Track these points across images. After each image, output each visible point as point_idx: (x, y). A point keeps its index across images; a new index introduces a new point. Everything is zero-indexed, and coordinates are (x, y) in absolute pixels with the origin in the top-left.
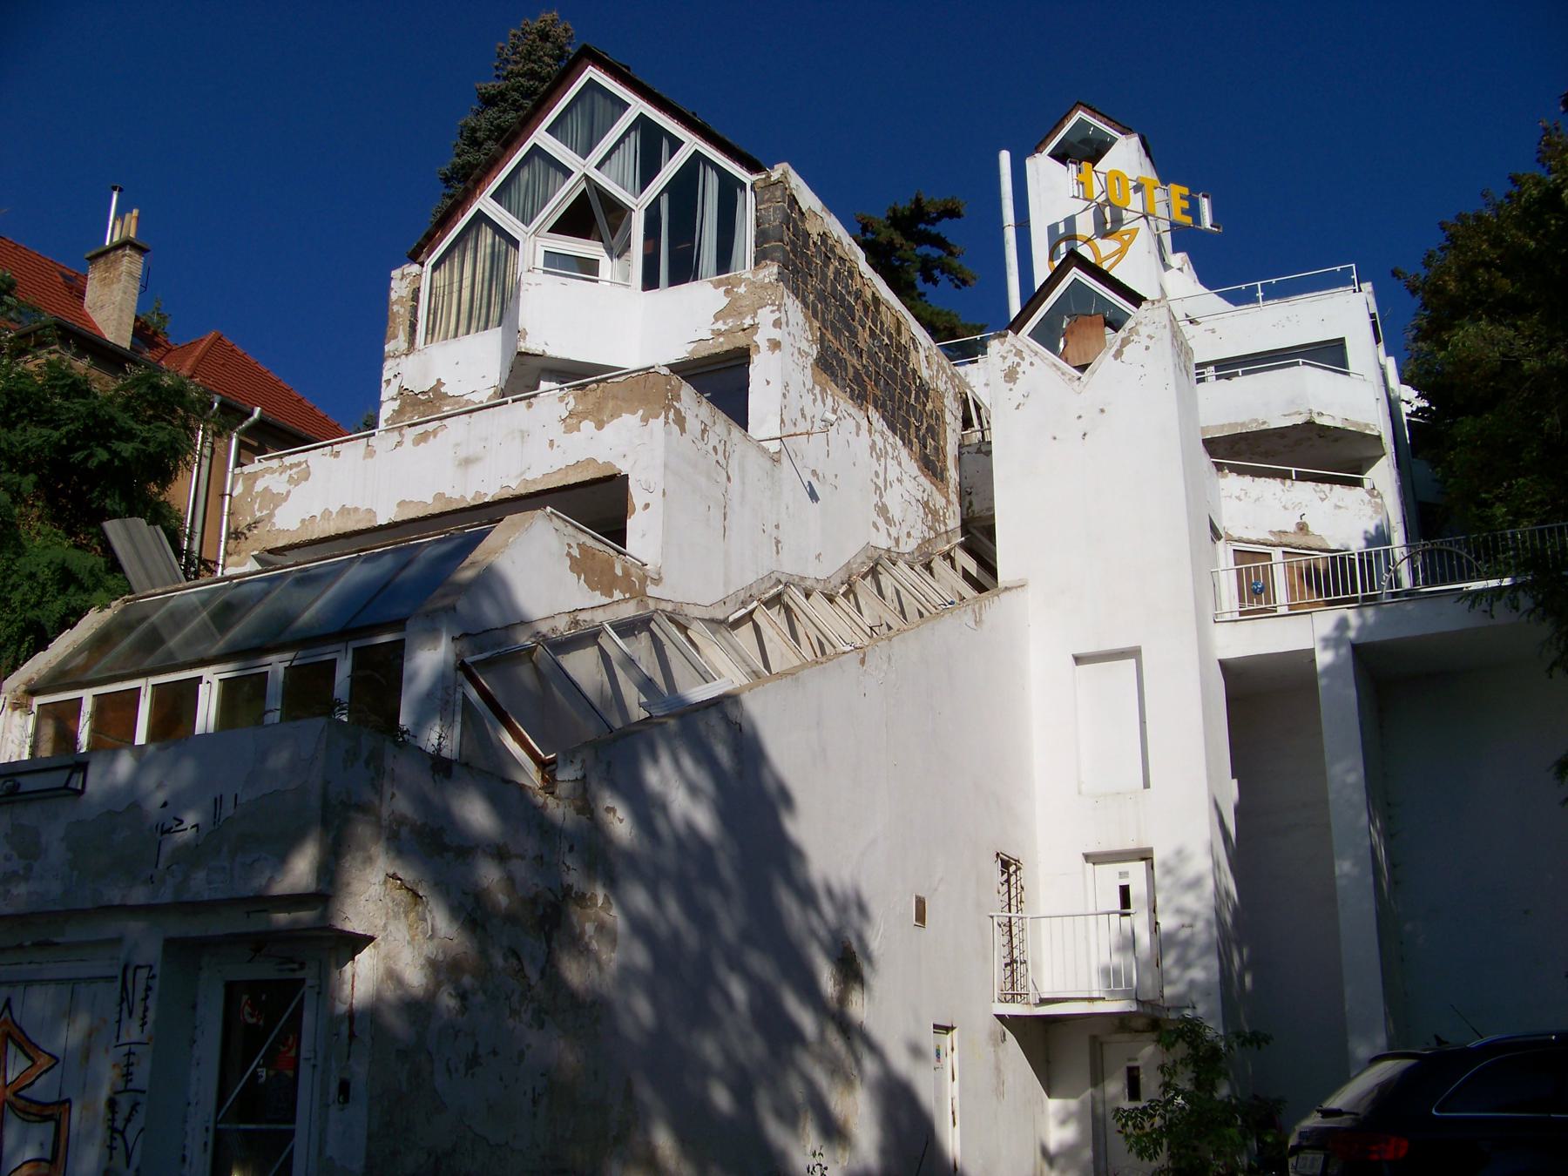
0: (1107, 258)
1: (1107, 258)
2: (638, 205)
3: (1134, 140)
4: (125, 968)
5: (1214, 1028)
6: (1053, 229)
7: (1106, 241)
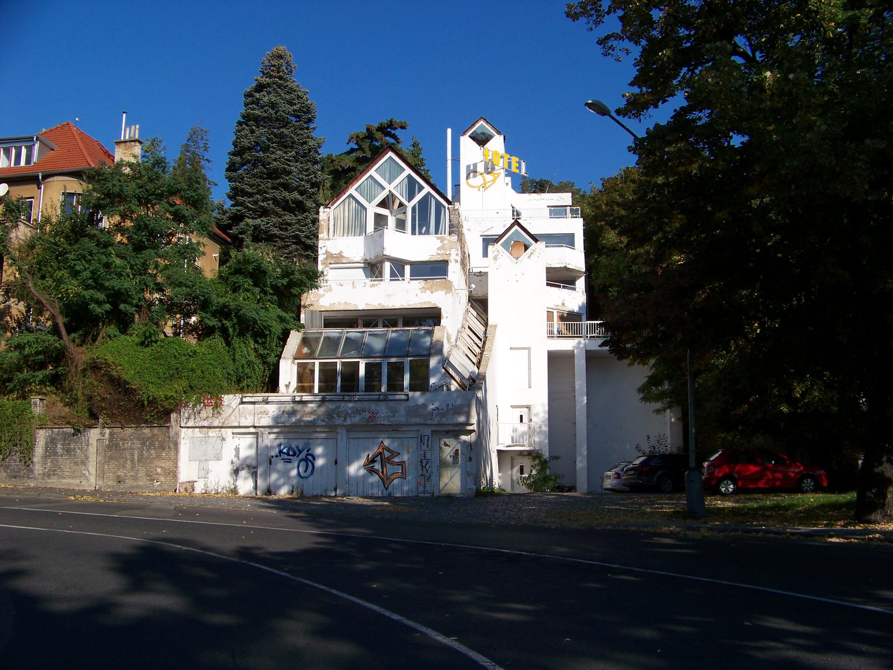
0: (488, 182)
1: (488, 182)
2: (410, 206)
3: (502, 137)
4: (421, 436)
5: (546, 455)
6: (468, 167)
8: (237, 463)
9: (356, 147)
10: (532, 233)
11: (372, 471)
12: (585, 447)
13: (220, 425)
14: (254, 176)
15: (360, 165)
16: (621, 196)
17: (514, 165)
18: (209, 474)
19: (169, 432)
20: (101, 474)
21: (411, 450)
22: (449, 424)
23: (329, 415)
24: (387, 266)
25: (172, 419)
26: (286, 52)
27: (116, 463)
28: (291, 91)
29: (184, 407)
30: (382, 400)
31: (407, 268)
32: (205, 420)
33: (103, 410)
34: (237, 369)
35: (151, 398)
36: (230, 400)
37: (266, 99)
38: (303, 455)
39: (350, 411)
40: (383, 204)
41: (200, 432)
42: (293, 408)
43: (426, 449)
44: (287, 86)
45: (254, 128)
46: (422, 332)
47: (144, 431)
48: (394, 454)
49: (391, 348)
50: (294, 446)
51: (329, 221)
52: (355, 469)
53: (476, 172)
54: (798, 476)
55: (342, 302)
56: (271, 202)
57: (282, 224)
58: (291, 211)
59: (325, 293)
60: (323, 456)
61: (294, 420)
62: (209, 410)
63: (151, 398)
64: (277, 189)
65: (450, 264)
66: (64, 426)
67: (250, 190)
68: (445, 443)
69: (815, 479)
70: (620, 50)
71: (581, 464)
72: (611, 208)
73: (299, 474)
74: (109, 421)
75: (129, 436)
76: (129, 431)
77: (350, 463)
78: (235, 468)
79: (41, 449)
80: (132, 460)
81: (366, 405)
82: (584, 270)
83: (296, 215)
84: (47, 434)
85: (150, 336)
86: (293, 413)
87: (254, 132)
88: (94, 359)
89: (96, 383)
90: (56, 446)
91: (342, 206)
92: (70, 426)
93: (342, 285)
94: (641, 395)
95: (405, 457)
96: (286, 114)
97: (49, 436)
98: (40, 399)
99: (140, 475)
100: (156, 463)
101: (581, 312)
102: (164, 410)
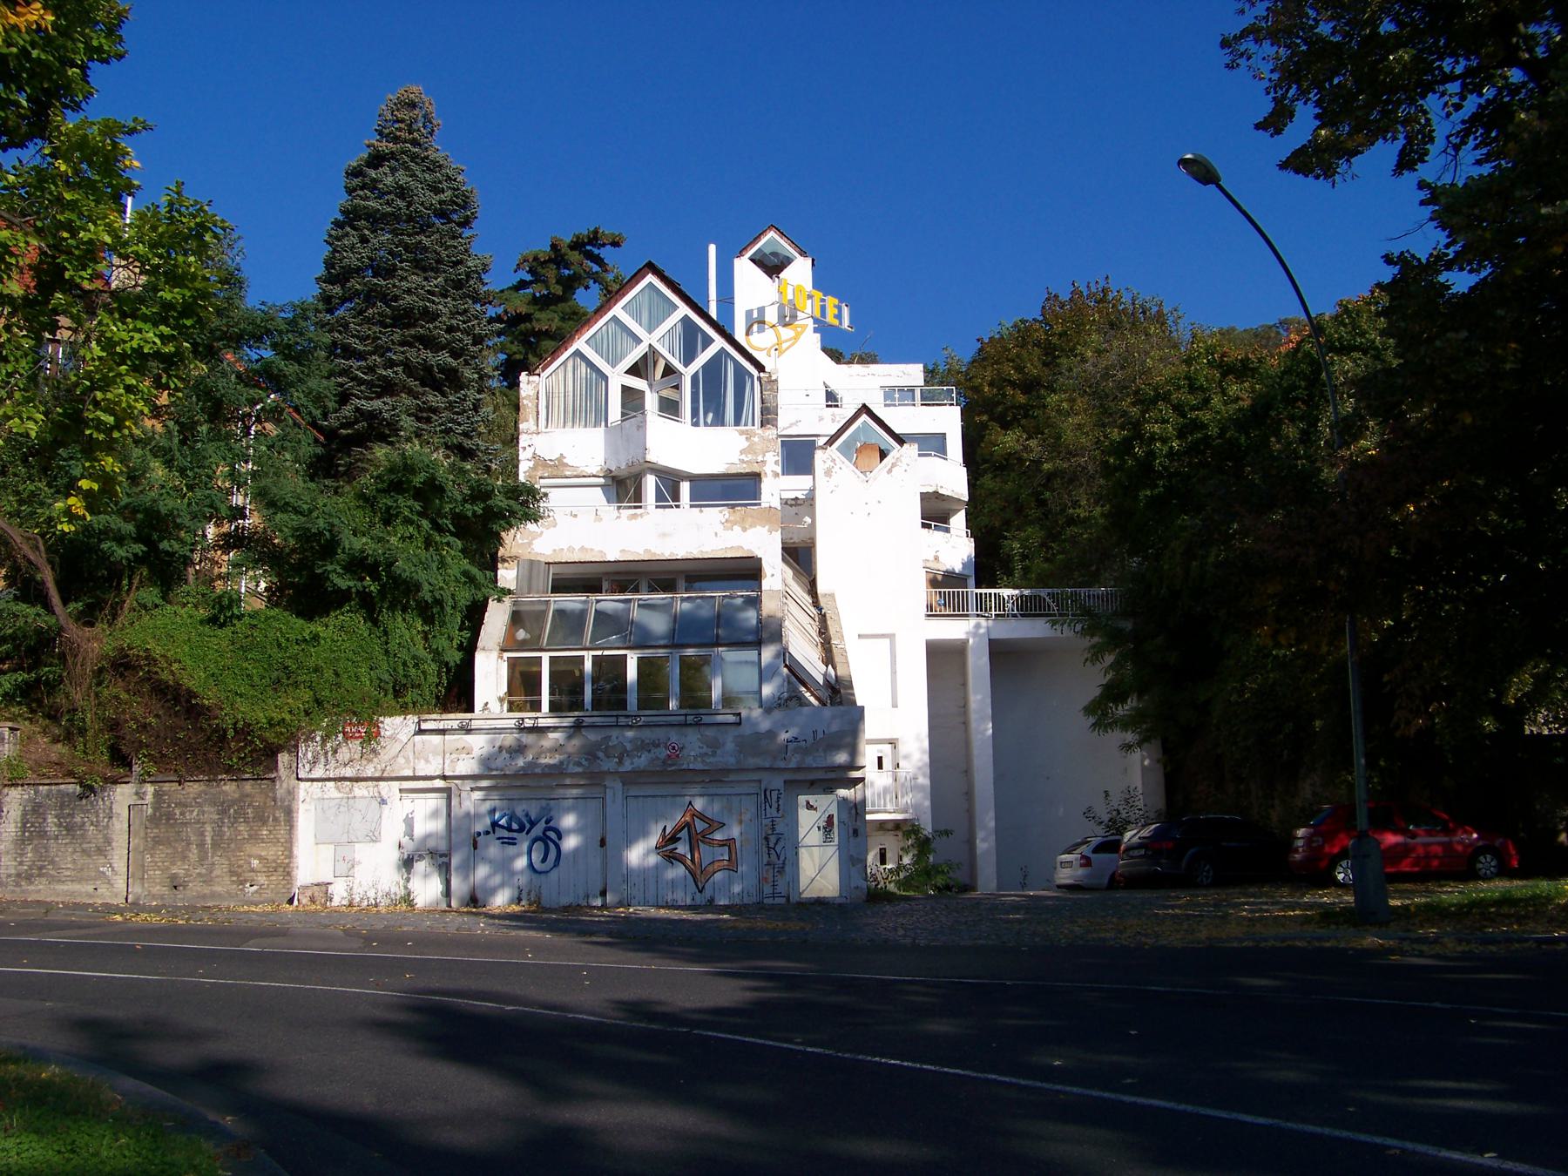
0: (786, 341)
1: (786, 341)
2: (688, 372)
3: (809, 261)
5: (927, 828)
6: (749, 313)
7: (784, 329)
8: (409, 846)
9: (528, 278)
10: (897, 432)
11: (671, 858)
12: (992, 814)
13: (377, 775)
14: (368, 320)
15: (541, 310)
16: (1020, 369)
17: (831, 312)
18: (356, 869)
19: (273, 790)
20: (136, 871)
21: (746, 817)
22: (817, 768)
23: (590, 753)
24: (650, 482)
25: (280, 764)
26: (423, 96)
27: (169, 851)
28: (435, 166)
29: (306, 741)
30: (691, 724)
31: (685, 487)
32: (345, 765)
33: (141, 748)
34: (395, 670)
35: (240, 725)
36: (397, 727)
37: (389, 180)
38: (538, 830)
39: (629, 746)
40: (634, 371)
41: (337, 788)
42: (518, 740)
43: (775, 814)
44: (427, 157)
45: (367, 232)
46: (739, 601)
47: (224, 788)
48: (715, 824)
49: (684, 631)
50: (519, 812)
51: (538, 398)
52: (639, 854)
53: (763, 322)
54: (1470, 850)
55: (577, 548)
56: (400, 369)
57: (421, 410)
58: (437, 387)
59: (544, 530)
60: (577, 830)
61: (521, 762)
62: (355, 745)
63: (240, 725)
64: (411, 345)
65: (764, 479)
66: (61, 781)
67: (361, 348)
68: (808, 803)
69: (1500, 855)
70: (1264, 59)
71: (984, 844)
72: (999, 390)
73: (531, 864)
74: (153, 770)
75: (195, 799)
76: (193, 788)
77: (629, 842)
78: (406, 857)
79: (13, 825)
80: (201, 845)
81: (659, 733)
82: (966, 499)
83: (444, 394)
84: (26, 797)
85: (230, 607)
86: (520, 749)
87: (367, 241)
88: (123, 649)
89: (124, 696)
90: (45, 819)
91: (561, 372)
92: (73, 780)
93: (576, 516)
94: (1092, 720)
95: (735, 832)
96: (426, 209)
97: (29, 800)
98: (10, 728)
99: (217, 872)
100: (250, 849)
101: (966, 572)
102: (265, 747)
